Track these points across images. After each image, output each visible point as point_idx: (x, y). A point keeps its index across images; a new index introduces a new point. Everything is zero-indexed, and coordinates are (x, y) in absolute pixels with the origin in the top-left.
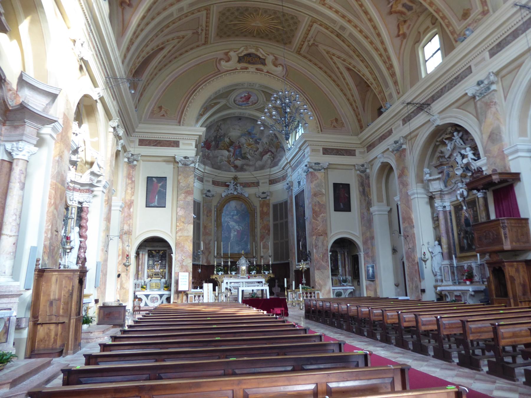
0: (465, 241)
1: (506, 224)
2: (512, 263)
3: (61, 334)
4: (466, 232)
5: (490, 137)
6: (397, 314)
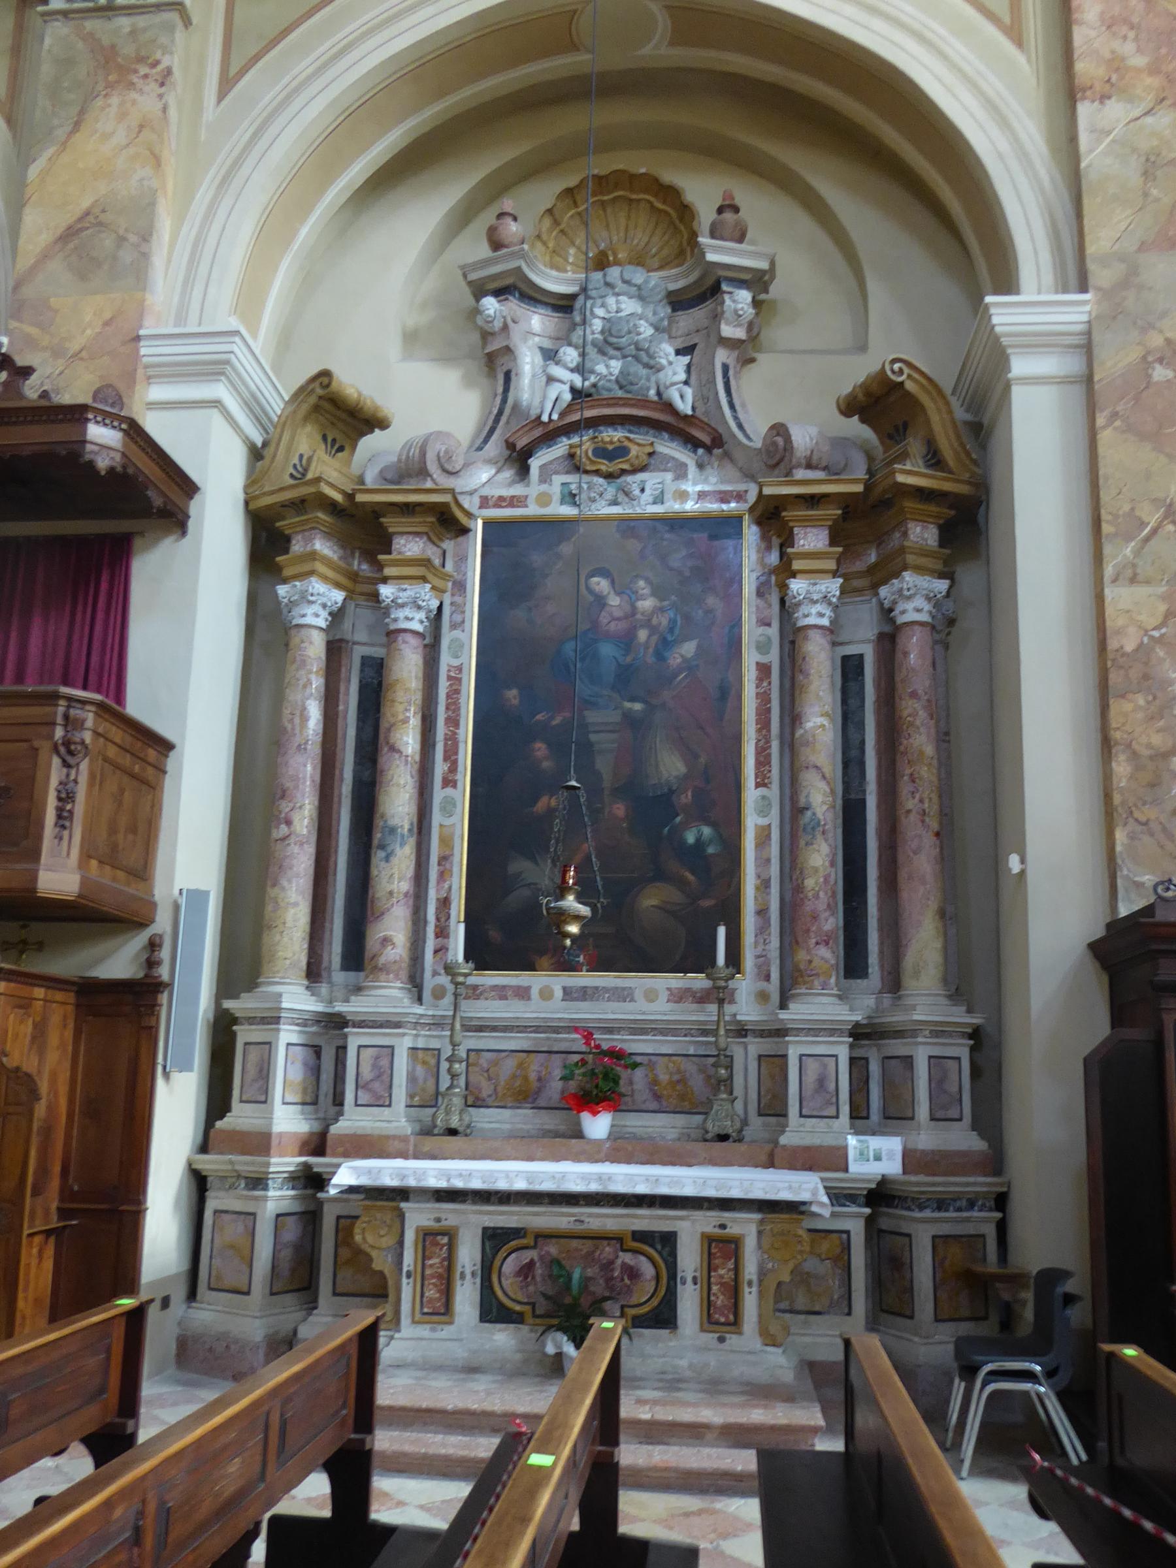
1: (88, 737)
2: (23, 990)
3: (762, 1273)
5: (70, 234)
6: (37, 1240)
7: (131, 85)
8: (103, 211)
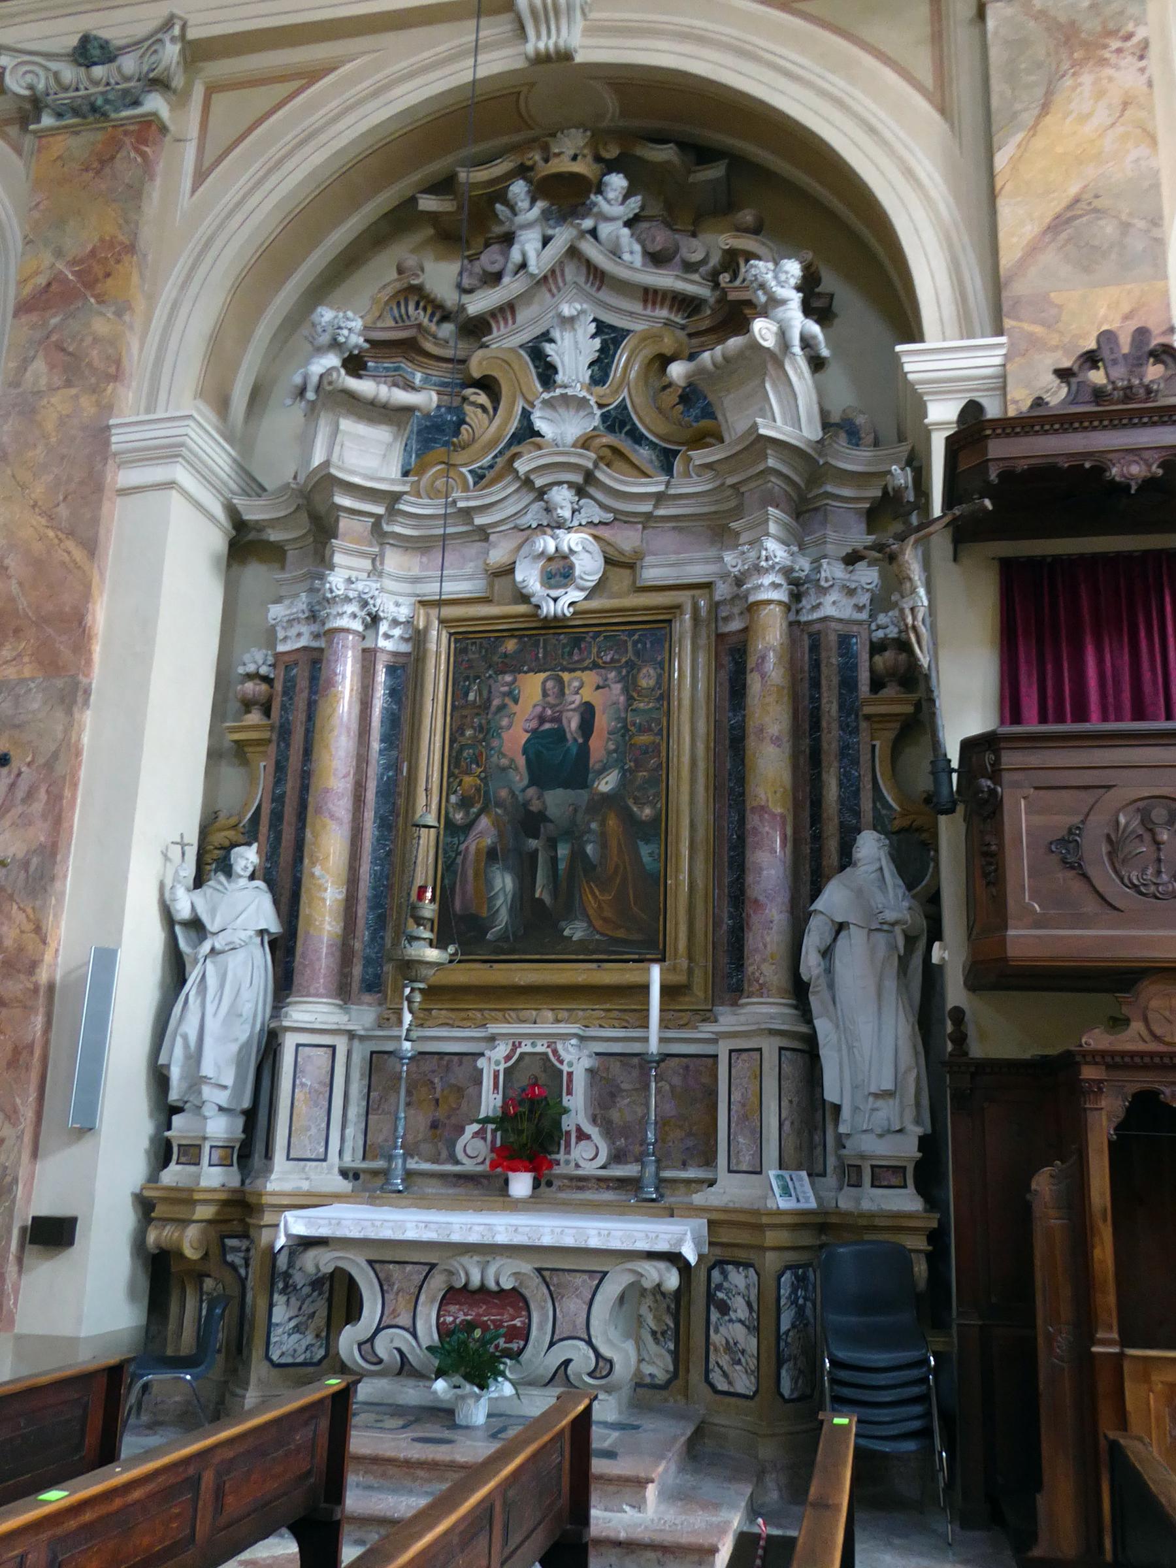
0: (504, 883)
4: (530, 822)
5: (1057, 225)
7: (1103, 62)
8: (1097, 197)
